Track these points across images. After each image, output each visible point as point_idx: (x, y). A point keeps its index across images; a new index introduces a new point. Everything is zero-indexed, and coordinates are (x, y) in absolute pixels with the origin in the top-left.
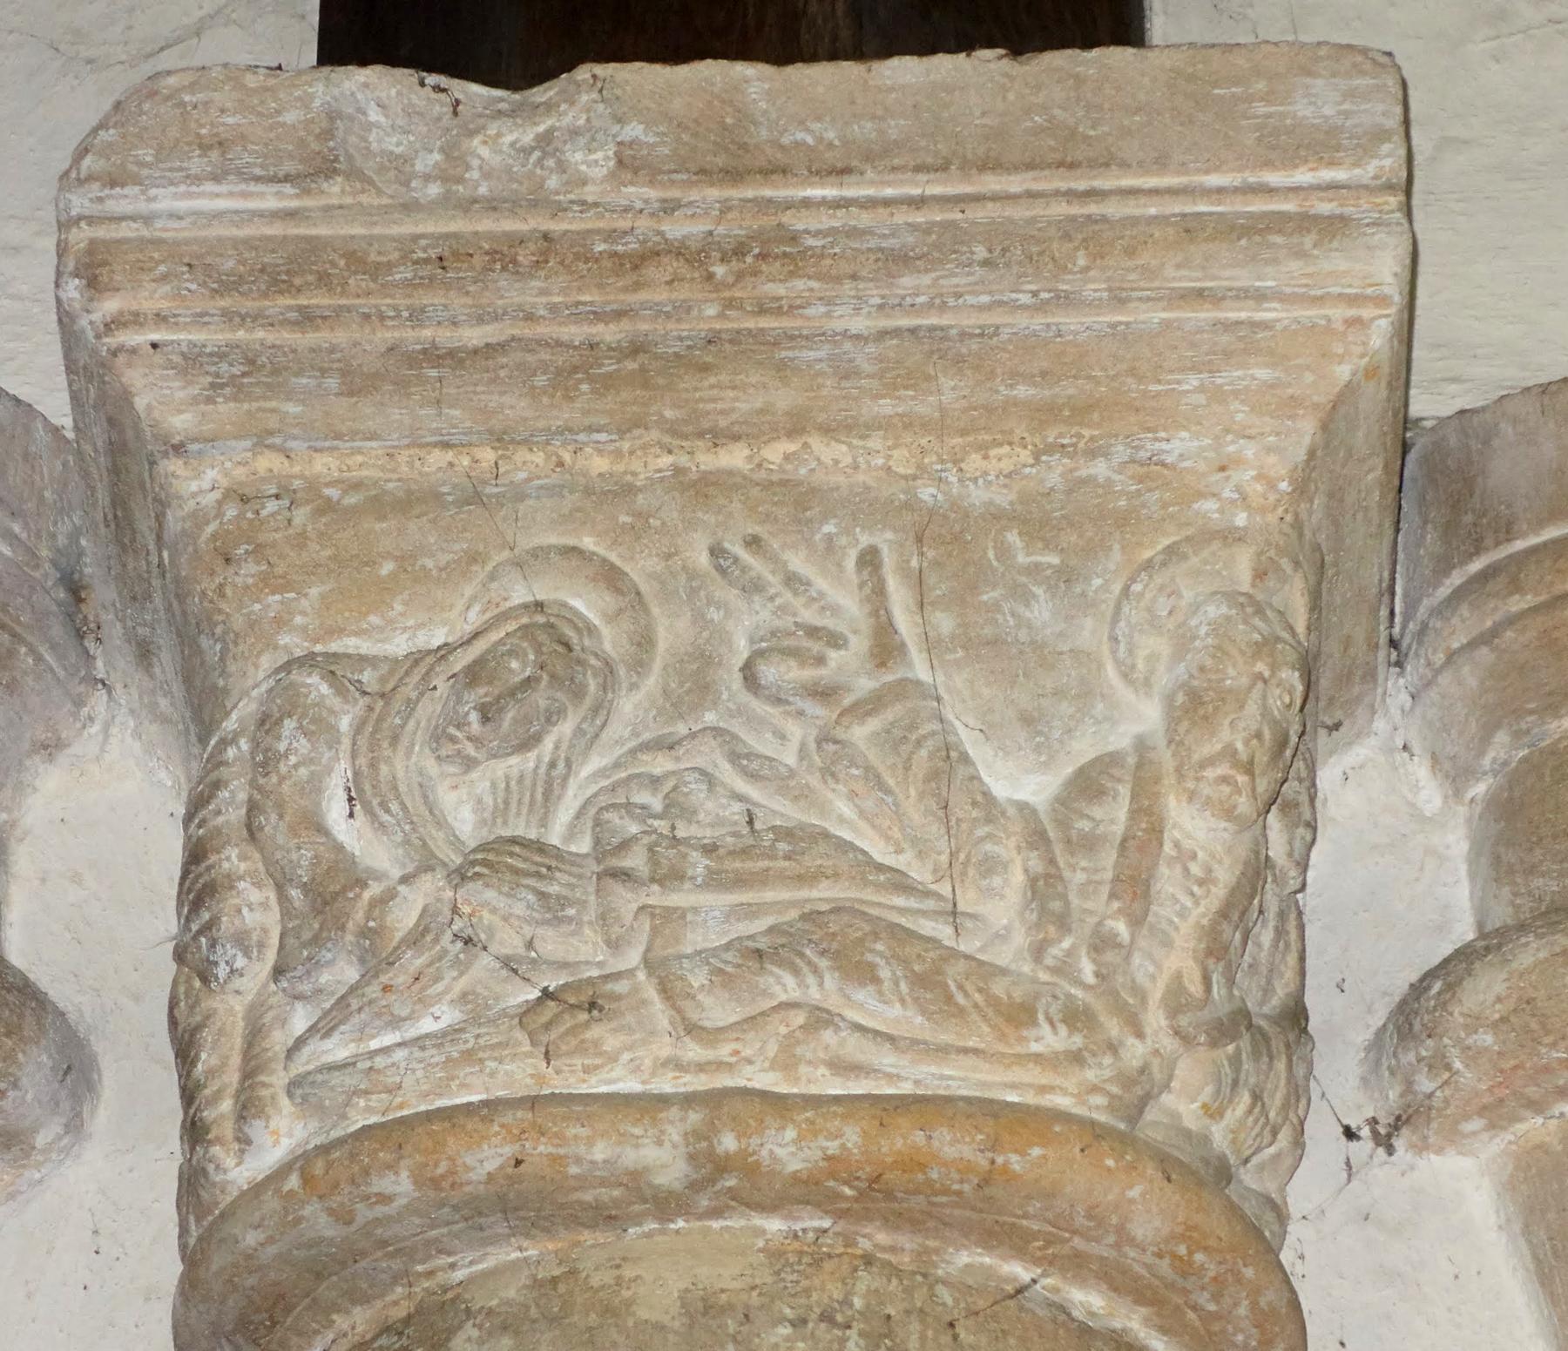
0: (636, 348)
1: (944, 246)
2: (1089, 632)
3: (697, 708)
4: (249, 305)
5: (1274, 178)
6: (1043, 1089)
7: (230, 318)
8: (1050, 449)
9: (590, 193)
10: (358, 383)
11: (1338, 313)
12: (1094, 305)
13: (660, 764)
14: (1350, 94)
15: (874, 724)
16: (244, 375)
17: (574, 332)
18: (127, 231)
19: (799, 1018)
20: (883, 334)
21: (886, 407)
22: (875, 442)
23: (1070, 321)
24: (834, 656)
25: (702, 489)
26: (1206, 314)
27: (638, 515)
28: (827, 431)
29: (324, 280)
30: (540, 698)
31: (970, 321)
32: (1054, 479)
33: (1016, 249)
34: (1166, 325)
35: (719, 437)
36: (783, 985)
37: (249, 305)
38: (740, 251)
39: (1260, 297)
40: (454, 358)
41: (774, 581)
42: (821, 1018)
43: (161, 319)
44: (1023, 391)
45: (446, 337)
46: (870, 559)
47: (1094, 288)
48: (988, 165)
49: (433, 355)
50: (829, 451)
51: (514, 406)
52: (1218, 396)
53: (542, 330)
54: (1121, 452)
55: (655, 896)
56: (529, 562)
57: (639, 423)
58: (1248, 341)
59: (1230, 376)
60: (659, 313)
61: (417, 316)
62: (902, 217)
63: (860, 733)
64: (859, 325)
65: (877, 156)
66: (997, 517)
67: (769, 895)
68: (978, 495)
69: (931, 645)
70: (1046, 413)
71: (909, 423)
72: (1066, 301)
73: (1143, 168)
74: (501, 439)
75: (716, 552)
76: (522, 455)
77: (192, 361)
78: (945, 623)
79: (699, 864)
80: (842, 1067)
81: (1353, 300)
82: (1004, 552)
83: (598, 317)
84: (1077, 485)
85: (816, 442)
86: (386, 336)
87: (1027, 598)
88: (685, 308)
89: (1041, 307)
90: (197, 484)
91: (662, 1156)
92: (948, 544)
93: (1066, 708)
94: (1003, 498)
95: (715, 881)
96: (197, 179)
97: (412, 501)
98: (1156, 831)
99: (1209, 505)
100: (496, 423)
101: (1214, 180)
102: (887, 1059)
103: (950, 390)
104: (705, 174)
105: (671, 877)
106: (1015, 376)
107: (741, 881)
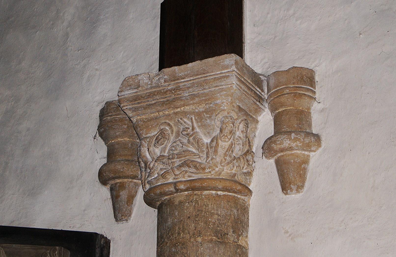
0: (168, 101)
1: (193, 85)
2: (213, 123)
3: (178, 137)
4: (134, 103)
5: (223, 71)
6: (207, 176)
7: (132, 104)
8: (207, 104)
9: (162, 84)
10: (145, 108)
11: (230, 86)
12: (208, 89)
13: (175, 144)
14: (230, 60)
15: (192, 137)
16: (135, 110)
17: (162, 100)
18: (123, 97)
19: (185, 172)
20: (189, 95)
21: (191, 102)
22: (191, 106)
23: (205, 91)
24: (189, 130)
25: (176, 114)
26: (217, 88)
27: (171, 117)
28: (187, 106)
29: (139, 99)
30: (162, 140)
31: (197, 93)
32: (208, 107)
33: (200, 85)
34: (214, 90)
35: (177, 108)
36: (183, 169)
37: (134, 103)
38: (175, 89)
39: (222, 85)
40: (152, 104)
41: (183, 123)
42: (186, 172)
43: (126, 106)
44: (204, 98)
45: (151, 103)
46: (191, 119)
47: (207, 87)
48: (197, 75)
49: (150, 105)
50: (187, 108)
51: (159, 108)
52: (221, 96)
53: (159, 100)
54: (213, 103)
55: (173, 161)
56: (162, 124)
57: (170, 108)
58: (222, 90)
59: (222, 93)
60: (169, 97)
61: (148, 101)
62: (189, 82)
63: (191, 138)
64: (187, 95)
65: (187, 76)
66: (203, 112)
67: (183, 158)
68: (201, 110)
69: (199, 127)
70: (206, 100)
71: (194, 103)
72: (205, 89)
73: (211, 73)
74: (158, 112)
75: (178, 120)
76: (160, 113)
77: (130, 109)
78: (200, 124)
79: (176, 157)
80: (189, 176)
81: (231, 84)
82: (204, 116)
83: (164, 98)
84: (210, 107)
85: (186, 107)
86: (146, 103)
87: (207, 120)
88: (171, 96)
89: (203, 90)
90: (134, 120)
91: (172, 189)
92: (199, 116)
93: (212, 131)
94: (203, 110)
95: (177, 158)
96: (128, 90)
97: (152, 119)
98: (218, 145)
99: (222, 107)
100: (158, 110)
101: (218, 73)
102: (193, 175)
103: (197, 99)
104: (172, 81)
105: (173, 158)
106: (202, 97)
107: (180, 158)
